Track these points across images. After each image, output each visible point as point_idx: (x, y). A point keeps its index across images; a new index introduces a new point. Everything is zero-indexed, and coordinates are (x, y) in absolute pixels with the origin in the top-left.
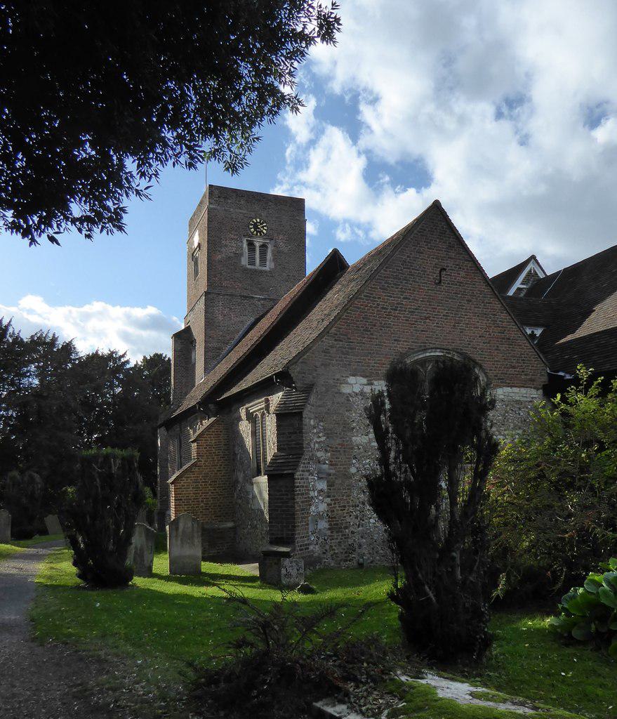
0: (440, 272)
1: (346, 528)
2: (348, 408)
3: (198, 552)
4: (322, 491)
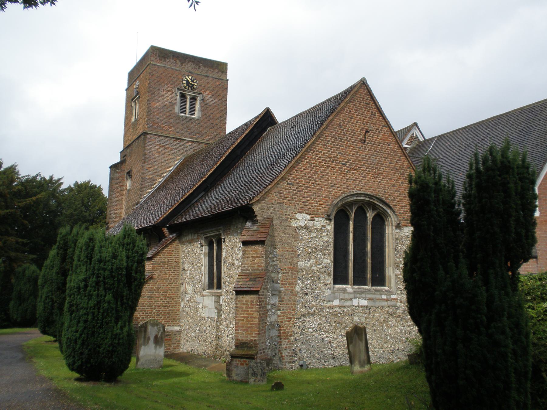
0: (365, 135)
1: (291, 335)
2: (296, 239)
4: (274, 305)
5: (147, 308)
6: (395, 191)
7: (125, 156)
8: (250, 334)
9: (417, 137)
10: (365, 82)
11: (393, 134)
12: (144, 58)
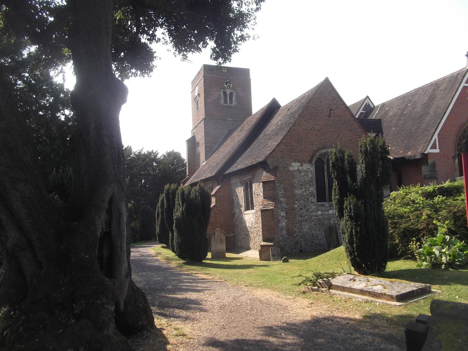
1: (294, 233)
4: (283, 216)
6: (351, 143)
7: (194, 133)
9: (370, 105)
11: (347, 109)
12: (200, 72)
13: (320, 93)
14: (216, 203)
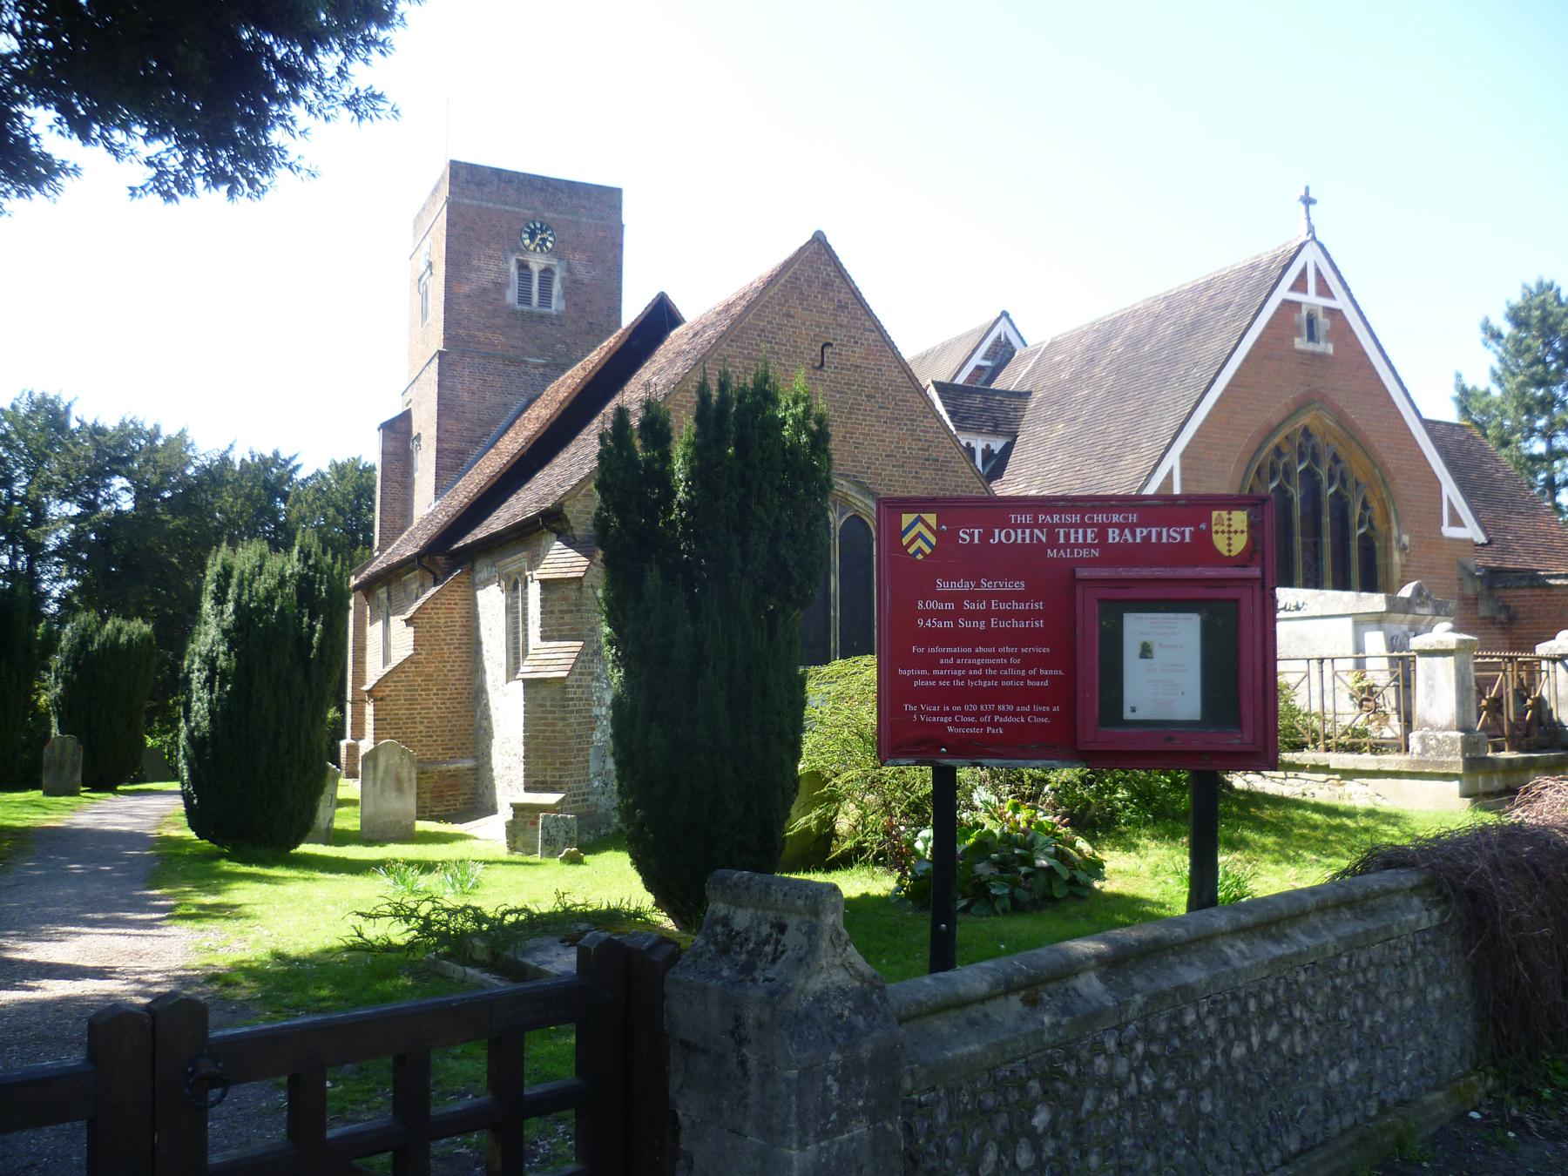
3: (410, 803)
5: (404, 723)
6: (893, 466)
8: (550, 764)
9: (1010, 343)
10: (822, 239)
13: (791, 283)
14: (415, 649)
